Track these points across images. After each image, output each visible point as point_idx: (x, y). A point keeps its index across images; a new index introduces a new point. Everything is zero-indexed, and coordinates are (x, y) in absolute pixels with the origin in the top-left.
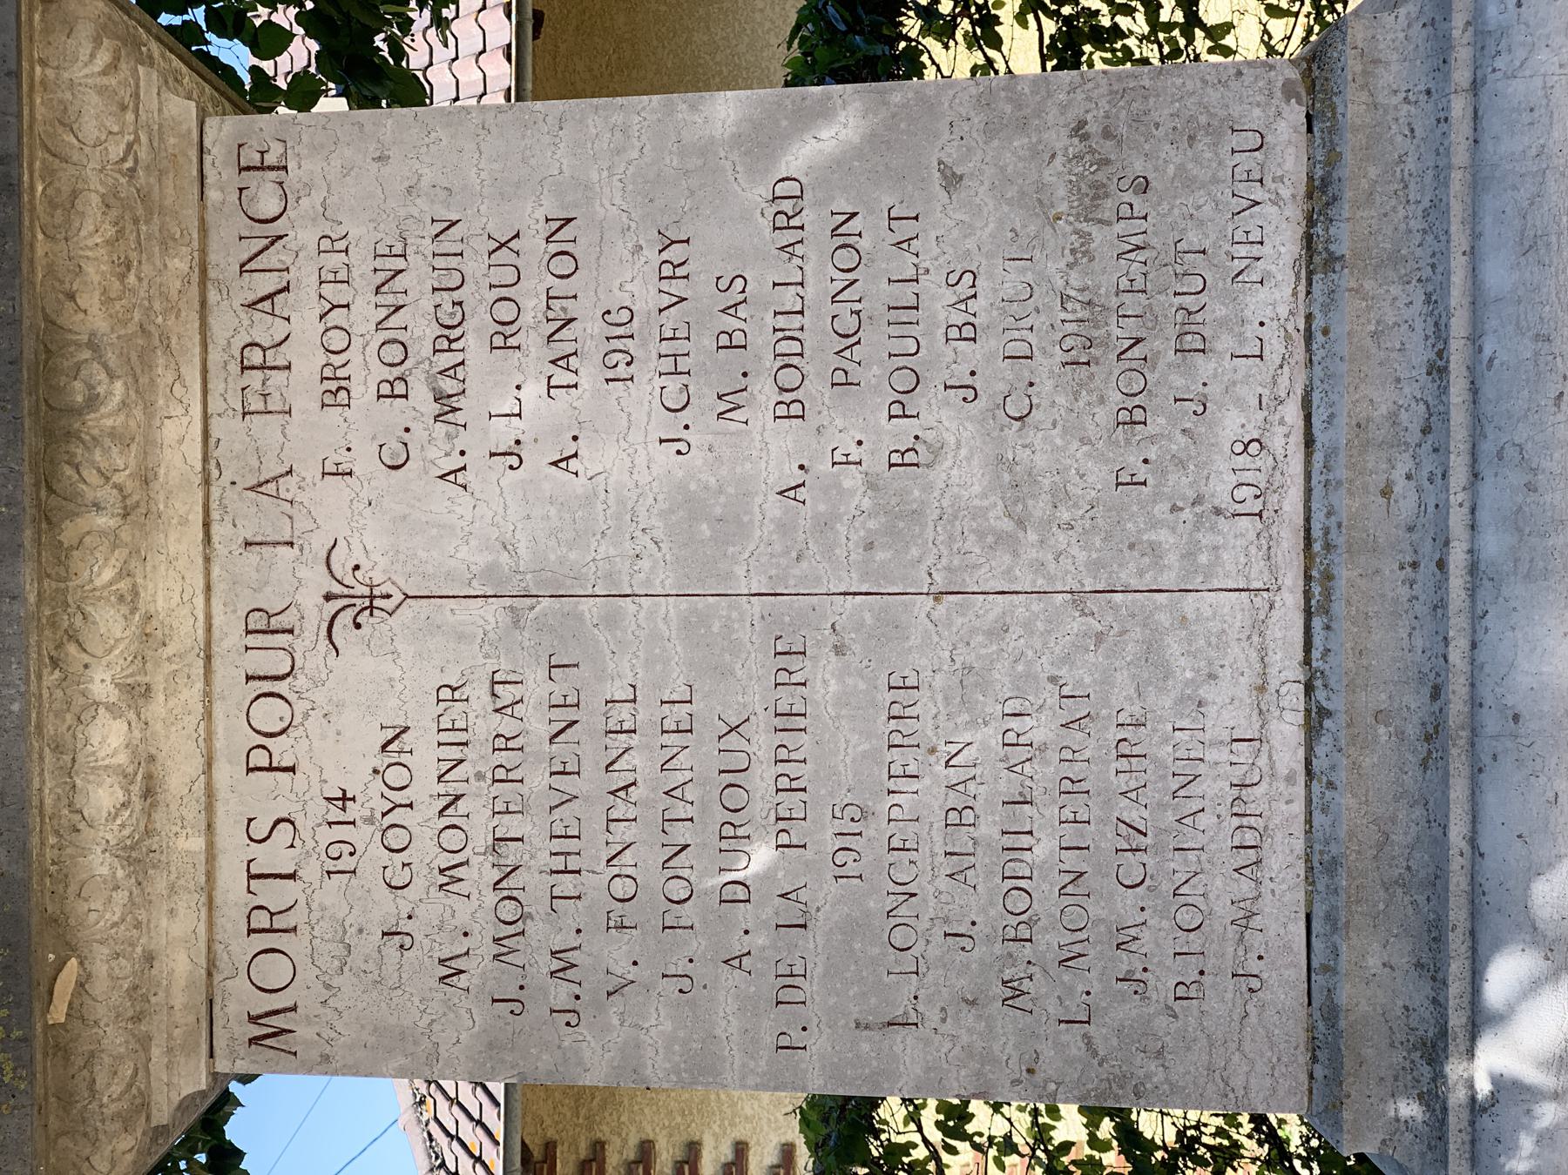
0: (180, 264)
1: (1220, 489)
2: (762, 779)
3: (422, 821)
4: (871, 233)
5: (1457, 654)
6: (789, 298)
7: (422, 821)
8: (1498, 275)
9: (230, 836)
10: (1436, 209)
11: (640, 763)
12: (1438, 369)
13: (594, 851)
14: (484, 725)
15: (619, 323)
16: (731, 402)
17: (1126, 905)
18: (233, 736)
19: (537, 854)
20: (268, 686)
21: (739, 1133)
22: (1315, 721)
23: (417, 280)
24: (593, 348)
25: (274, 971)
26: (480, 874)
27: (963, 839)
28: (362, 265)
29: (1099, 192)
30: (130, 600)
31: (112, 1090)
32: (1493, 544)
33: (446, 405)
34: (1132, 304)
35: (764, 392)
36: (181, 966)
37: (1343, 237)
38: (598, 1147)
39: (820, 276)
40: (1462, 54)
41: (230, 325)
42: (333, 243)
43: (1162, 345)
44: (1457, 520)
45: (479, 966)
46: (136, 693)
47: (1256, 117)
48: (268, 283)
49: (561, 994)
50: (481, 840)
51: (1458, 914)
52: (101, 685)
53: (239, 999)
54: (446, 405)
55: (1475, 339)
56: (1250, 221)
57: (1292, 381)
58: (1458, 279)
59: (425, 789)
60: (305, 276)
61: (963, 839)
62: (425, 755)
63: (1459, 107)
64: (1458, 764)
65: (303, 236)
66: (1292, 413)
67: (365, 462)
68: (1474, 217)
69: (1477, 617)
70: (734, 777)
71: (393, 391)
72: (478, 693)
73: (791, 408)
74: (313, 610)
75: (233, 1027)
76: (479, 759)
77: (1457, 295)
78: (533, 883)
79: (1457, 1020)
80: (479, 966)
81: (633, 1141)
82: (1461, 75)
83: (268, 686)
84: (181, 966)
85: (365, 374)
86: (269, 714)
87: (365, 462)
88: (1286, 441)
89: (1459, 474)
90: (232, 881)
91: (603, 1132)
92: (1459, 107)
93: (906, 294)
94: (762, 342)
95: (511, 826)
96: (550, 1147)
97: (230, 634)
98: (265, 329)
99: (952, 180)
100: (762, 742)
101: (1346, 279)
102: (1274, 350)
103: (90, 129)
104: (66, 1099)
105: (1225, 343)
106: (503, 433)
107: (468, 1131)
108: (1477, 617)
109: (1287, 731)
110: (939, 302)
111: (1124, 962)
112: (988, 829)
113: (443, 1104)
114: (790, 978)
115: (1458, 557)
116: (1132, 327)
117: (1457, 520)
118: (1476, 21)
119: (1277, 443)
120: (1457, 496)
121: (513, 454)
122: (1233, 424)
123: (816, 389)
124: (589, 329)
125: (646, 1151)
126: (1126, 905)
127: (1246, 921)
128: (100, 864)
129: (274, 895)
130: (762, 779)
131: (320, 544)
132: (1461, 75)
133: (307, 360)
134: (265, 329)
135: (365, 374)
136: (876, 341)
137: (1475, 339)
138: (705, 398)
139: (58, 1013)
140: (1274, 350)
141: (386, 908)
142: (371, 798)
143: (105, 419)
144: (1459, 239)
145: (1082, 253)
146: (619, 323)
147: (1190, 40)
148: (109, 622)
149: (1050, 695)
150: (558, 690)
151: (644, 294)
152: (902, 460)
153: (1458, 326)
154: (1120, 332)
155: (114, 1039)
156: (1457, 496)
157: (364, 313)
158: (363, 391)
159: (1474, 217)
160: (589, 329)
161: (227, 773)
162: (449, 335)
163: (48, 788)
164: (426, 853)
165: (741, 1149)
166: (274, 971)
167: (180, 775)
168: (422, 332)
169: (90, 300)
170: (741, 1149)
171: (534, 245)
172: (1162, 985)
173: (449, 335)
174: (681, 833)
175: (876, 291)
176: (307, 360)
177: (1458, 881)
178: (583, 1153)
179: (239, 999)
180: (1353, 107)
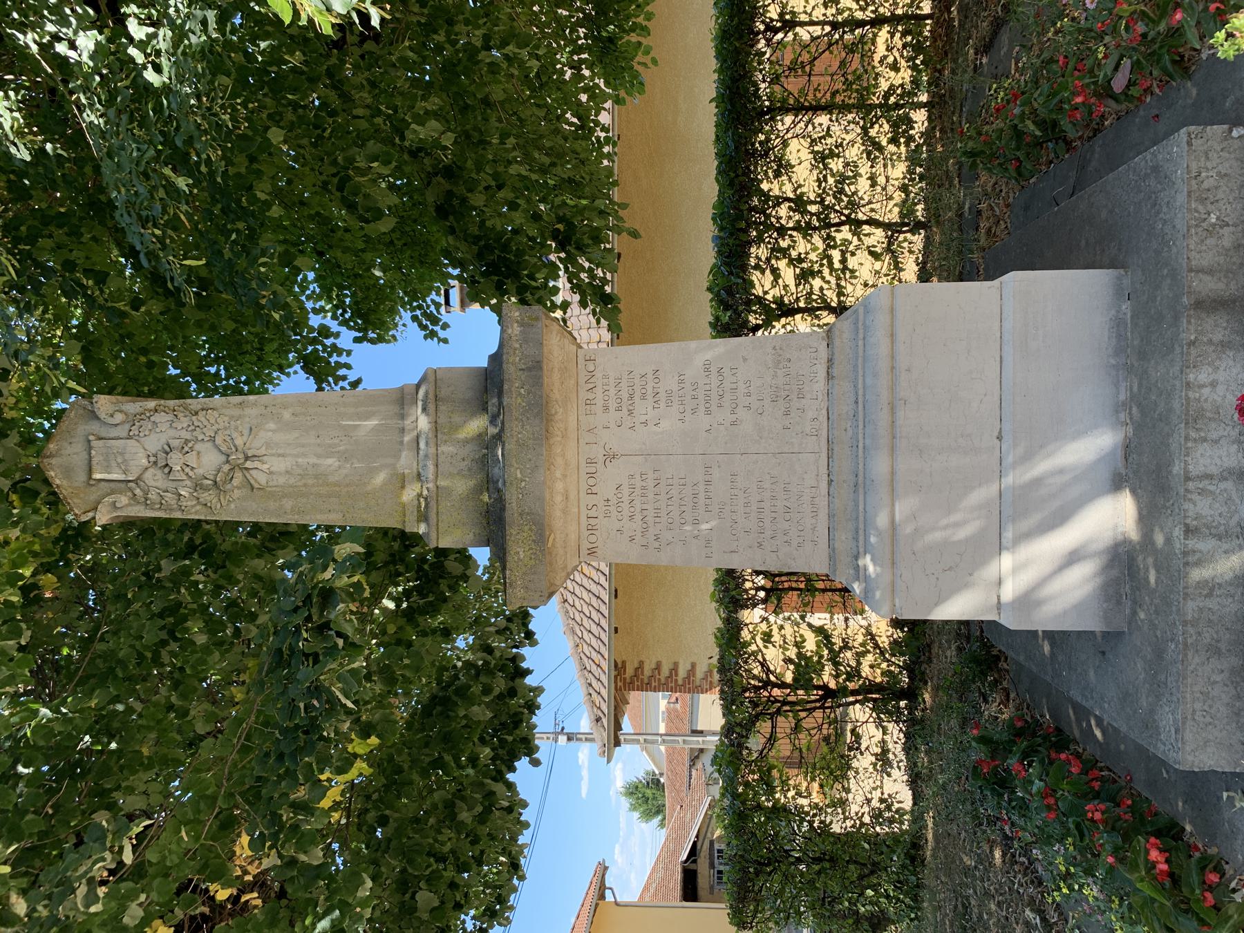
0: (573, 382)
1: (807, 430)
2: (702, 496)
3: (625, 506)
4: (726, 372)
5: (861, 466)
6: (708, 387)
7: (625, 506)
8: (869, 381)
9: (583, 508)
10: (856, 366)
11: (674, 492)
12: (856, 402)
13: (663, 513)
14: (639, 484)
15: (669, 394)
16: (694, 411)
17: (786, 525)
18: (584, 487)
19: (651, 514)
20: (591, 475)
21: (694, 659)
22: (830, 482)
23: (624, 385)
24: (663, 399)
25: (593, 539)
26: (638, 517)
27: (748, 510)
28: (612, 381)
29: (779, 362)
30: (564, 456)
31: (560, 562)
32: (868, 441)
33: (630, 412)
34: (787, 387)
35: (702, 409)
36: (573, 537)
37: (835, 372)
38: (641, 663)
39: (715, 381)
40: (861, 331)
41: (584, 395)
42: (606, 377)
43: (794, 396)
44: (861, 436)
45: (638, 538)
46: (565, 476)
47: (815, 345)
48: (591, 386)
49: (656, 544)
50: (638, 509)
51: (861, 526)
52: (558, 474)
53: (585, 545)
54: (630, 412)
55: (864, 395)
56: (814, 368)
57: (824, 405)
58: (860, 382)
59: (626, 498)
60: (599, 384)
61: (748, 510)
62: (626, 490)
63: (861, 343)
64: (861, 491)
65: (599, 374)
66: (825, 412)
67: (612, 425)
68: (864, 368)
69: (865, 458)
70: (695, 495)
71: (619, 409)
72: (638, 476)
73: (708, 412)
74: (602, 459)
75: (584, 552)
76: (638, 491)
77: (860, 386)
78: (650, 519)
79: (861, 550)
80: (638, 538)
81: (654, 661)
82: (861, 336)
83: (591, 475)
84: (573, 537)
85: (613, 405)
86: (591, 482)
87: (612, 425)
88: (823, 418)
89: (861, 427)
90: (583, 518)
91: (643, 658)
92: (861, 343)
93: (734, 386)
94: (701, 397)
95: (645, 507)
96: (624, 662)
97: (583, 464)
98: (591, 396)
99: (745, 360)
100: (701, 487)
101: (836, 382)
102: (820, 398)
103: (556, 354)
104: (551, 564)
105: (809, 396)
106: (643, 419)
107: (594, 655)
108: (865, 458)
109: (824, 485)
110: (742, 386)
111: (786, 538)
112: (754, 508)
113: (585, 646)
114: (708, 541)
115: (861, 445)
116: (787, 393)
117: (861, 436)
118: (864, 324)
119: (821, 419)
120: (861, 431)
121: (645, 423)
122: (810, 414)
123: (714, 408)
124: (662, 396)
125: (658, 667)
126: (786, 525)
127: (814, 529)
128: (558, 513)
129: (592, 521)
130: (702, 496)
131: (602, 444)
132: (861, 336)
133: (600, 402)
134: (591, 396)
135: (613, 405)
136: (727, 397)
137: (864, 395)
138: (689, 411)
139: (550, 545)
140: (820, 398)
141: (618, 525)
142: (614, 501)
143: (558, 417)
144: (861, 373)
145: (775, 376)
146: (669, 394)
147: (844, 274)
148: (559, 461)
149: (768, 477)
150: (655, 476)
151: (675, 387)
152: (733, 424)
153: (860, 392)
154: (783, 394)
155: (561, 552)
156: (861, 431)
157: (612, 392)
158: (612, 409)
159: (864, 368)
160: (662, 396)
161: (583, 494)
162: (631, 397)
163: (547, 496)
164: (626, 513)
165: (693, 665)
166: (593, 539)
167: (573, 495)
168: (625, 395)
169: (556, 391)
170: (693, 665)
171: (650, 376)
172: (794, 543)
173: (631, 397)
174: (683, 508)
175: (727, 385)
176: (600, 402)
177: (861, 518)
178: (636, 665)
179: (585, 545)
180: (837, 342)
